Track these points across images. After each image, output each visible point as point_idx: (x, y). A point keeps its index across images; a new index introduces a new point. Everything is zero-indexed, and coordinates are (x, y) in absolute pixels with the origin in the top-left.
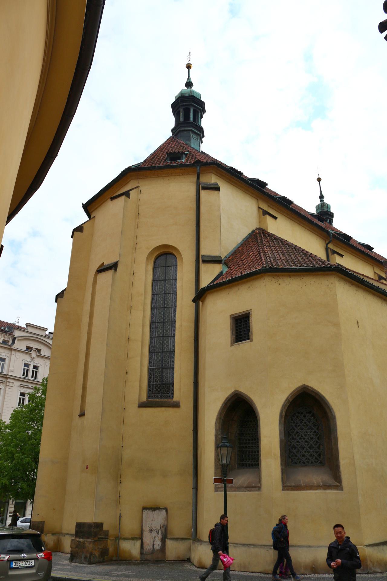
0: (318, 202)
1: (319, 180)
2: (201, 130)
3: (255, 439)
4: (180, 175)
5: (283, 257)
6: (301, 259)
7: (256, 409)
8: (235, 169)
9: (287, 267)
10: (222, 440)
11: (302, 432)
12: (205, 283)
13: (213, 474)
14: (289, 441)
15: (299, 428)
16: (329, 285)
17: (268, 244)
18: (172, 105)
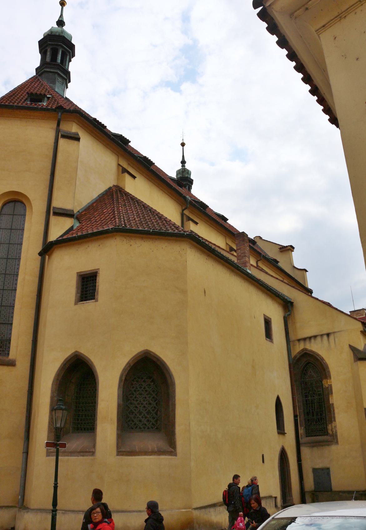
0: (179, 167)
1: (183, 145)
2: (68, 74)
3: (92, 403)
4: (39, 119)
5: (138, 218)
6: (155, 222)
7: (96, 372)
8: (98, 121)
9: (141, 228)
10: (57, 403)
11: (141, 397)
12: (53, 236)
13: (46, 438)
14: (127, 406)
15: (138, 393)
16: (181, 251)
17: (124, 203)
18: (39, 42)
